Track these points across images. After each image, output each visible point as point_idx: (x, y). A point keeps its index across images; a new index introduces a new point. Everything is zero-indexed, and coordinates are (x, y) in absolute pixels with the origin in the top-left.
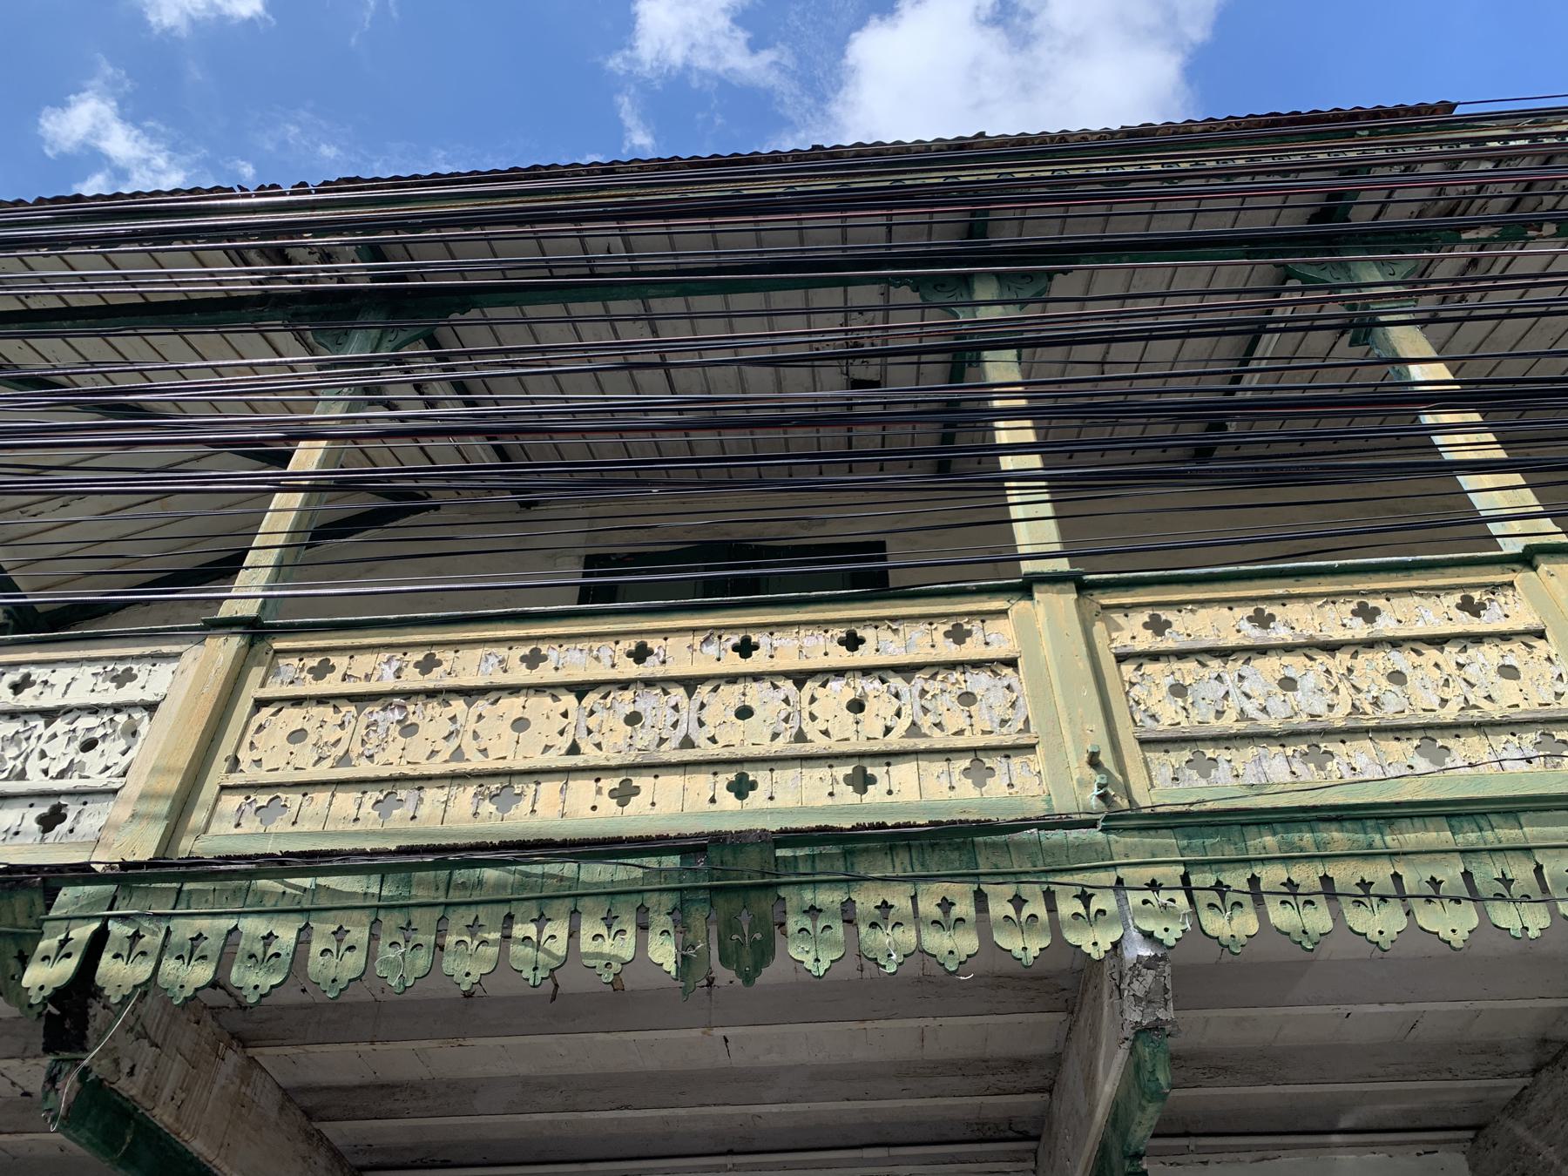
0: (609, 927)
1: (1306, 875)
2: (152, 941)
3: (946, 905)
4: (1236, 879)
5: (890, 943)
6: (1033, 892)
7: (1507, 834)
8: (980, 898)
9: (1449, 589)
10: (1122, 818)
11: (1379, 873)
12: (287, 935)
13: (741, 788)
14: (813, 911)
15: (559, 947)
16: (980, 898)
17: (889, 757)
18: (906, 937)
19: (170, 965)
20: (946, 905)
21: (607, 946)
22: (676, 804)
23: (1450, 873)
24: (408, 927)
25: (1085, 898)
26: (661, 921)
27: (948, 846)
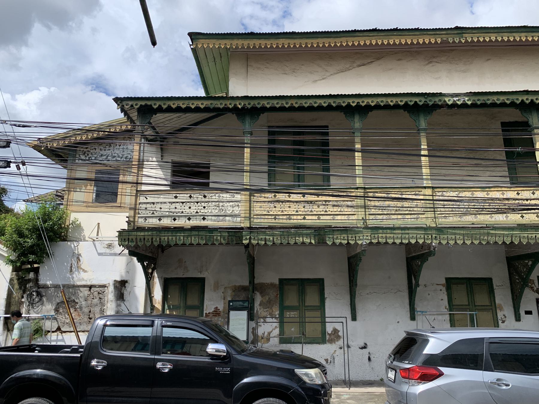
0: (46, 229)
1: (384, 235)
2: (256, 238)
3: (344, 237)
4: (376, 236)
5: (338, 242)
6: (354, 235)
7: (407, 232)
8: (348, 237)
9: (501, 191)
10: (367, 228)
11: (392, 235)
12: (271, 239)
13: (160, 220)
14: (329, 238)
15: (301, 240)
16: (348, 237)
17: (164, 217)
18: (339, 241)
19: (259, 242)
20: (344, 237)
21: (307, 241)
22: (311, 221)
23: (415, 236)
24: (284, 238)
25: (359, 237)
26: (313, 238)
27: (345, 230)
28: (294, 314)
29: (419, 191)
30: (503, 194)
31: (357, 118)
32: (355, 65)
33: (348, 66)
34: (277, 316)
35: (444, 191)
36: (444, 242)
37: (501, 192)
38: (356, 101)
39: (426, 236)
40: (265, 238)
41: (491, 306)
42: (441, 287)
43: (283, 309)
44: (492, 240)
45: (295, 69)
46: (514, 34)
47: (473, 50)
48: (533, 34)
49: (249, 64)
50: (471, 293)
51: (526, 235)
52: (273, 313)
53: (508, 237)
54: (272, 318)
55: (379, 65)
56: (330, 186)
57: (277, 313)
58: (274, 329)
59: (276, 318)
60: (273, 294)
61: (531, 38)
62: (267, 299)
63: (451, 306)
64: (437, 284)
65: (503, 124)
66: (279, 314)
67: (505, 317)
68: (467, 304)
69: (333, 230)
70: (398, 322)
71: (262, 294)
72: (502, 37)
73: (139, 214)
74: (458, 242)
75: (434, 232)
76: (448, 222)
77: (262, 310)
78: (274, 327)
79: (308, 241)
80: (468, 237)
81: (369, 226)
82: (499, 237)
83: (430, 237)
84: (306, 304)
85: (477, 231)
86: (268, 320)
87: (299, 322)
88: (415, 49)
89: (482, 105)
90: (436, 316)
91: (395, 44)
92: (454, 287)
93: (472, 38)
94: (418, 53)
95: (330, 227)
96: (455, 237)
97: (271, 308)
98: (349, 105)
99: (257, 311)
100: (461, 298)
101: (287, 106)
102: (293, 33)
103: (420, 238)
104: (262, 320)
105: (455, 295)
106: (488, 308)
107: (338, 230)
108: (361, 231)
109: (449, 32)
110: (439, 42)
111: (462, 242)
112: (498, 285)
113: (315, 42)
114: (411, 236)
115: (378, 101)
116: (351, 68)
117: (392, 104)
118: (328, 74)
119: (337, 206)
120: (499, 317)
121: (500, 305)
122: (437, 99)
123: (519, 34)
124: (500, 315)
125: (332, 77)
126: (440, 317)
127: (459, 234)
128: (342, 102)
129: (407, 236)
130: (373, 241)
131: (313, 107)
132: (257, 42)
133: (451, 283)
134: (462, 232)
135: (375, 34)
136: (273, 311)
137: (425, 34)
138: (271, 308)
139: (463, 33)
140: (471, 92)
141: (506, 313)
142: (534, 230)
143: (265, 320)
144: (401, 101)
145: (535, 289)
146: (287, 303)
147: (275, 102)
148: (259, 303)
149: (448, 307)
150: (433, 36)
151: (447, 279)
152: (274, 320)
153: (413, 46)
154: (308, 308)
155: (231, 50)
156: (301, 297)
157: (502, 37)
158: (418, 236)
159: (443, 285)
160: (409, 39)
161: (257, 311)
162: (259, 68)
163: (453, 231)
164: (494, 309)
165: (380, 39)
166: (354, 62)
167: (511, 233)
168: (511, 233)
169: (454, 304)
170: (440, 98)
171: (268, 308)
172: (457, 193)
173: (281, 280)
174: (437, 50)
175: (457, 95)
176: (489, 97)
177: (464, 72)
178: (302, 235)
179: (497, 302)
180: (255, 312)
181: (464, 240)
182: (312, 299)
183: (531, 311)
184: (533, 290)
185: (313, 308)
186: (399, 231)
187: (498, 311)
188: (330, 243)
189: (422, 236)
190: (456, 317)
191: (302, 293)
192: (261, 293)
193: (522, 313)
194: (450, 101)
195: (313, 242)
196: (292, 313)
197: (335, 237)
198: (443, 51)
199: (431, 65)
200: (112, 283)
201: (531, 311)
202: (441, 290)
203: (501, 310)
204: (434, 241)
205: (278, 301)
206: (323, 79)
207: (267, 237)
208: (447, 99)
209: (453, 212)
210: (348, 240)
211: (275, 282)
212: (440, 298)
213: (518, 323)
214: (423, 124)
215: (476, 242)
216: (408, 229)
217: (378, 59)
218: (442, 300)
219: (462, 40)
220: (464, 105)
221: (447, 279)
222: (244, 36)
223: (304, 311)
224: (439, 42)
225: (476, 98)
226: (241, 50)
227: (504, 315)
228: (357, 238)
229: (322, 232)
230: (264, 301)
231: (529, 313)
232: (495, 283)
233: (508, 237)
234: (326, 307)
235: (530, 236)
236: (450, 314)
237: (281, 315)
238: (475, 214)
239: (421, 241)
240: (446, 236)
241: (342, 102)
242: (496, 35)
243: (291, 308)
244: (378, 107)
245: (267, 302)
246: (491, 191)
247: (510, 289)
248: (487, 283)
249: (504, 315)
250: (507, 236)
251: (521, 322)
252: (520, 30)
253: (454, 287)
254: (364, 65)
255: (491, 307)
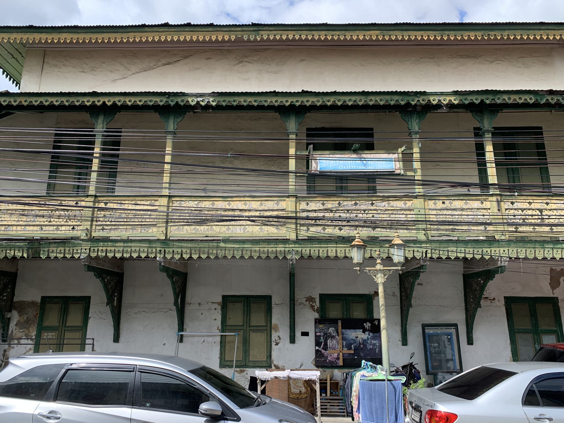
5: (52, 255)
6: (71, 248)
7: (130, 244)
14: (44, 251)
15: (13, 254)
18: (55, 255)
20: (60, 251)
21: (18, 254)
23: (138, 249)
25: (77, 250)
26: (25, 251)
27: (64, 241)
28: (52, 336)
29: (156, 200)
30: (277, 204)
31: (101, 119)
32: (160, 64)
33: (152, 65)
34: (34, 337)
35: (183, 201)
36: (169, 256)
37: (243, 202)
38: (92, 99)
39: (150, 250)
40: (106, 250)
41: (267, 326)
42: (216, 306)
43: (41, 329)
44: (221, 254)
45: (94, 67)
46: (314, 32)
47: (288, 49)
48: (333, 33)
49: (46, 61)
50: (247, 313)
51: (257, 249)
52: (29, 334)
53: (238, 250)
54: (28, 339)
55: (186, 64)
56: (376, 193)
57: (34, 334)
58: (28, 352)
59: (31, 339)
60: (32, 313)
61: (559, 37)
62: (25, 318)
63: (224, 327)
64: (213, 303)
65: (308, 129)
66: (36, 336)
67: (280, 339)
68: (242, 324)
69: (50, 243)
70: (164, 344)
71: (20, 313)
72: (300, 35)
73: (97, 221)
74: (184, 256)
75: (158, 245)
76: (180, 234)
77: (17, 331)
78: (28, 350)
79: (21, 254)
80: (195, 251)
81: (171, 238)
82: (229, 250)
83: (154, 250)
84: (251, 324)
85: (206, 245)
86: (22, 341)
87: (57, 344)
88: (226, 48)
89: (480, 106)
90: (206, 338)
91: (185, 40)
92: (230, 306)
93: (268, 35)
94: (229, 51)
95: (47, 239)
96: (182, 251)
97: (28, 329)
98: (408, 104)
99: (12, 331)
100: (236, 318)
101: (15, 104)
102: (76, 27)
103: (144, 252)
104: (16, 342)
105: (230, 315)
106: (239, 328)
107: (55, 242)
108: (81, 244)
109: (244, 29)
110: (233, 39)
111: (188, 256)
112: (277, 303)
113: (100, 37)
114: (133, 249)
115: (116, 100)
116: (155, 67)
117: (129, 104)
118: (130, 73)
119: (23, 215)
120: (273, 339)
121: (276, 325)
122: (179, 100)
123: (318, 32)
124: (274, 336)
125: (133, 75)
126: (210, 339)
127: (186, 247)
128: (75, 100)
129: (129, 249)
130: (67, 256)
131: (326, 105)
132: (37, 36)
133: (227, 301)
134: (189, 245)
135: (165, 29)
136: (29, 332)
137: (219, 31)
138: (28, 329)
139: (260, 30)
140: (213, 92)
141: (281, 334)
142: (273, 243)
143: (19, 342)
144: (140, 101)
145: (316, 308)
146: (46, 323)
147: (137, 99)
148: (15, 323)
149: (220, 328)
150: (227, 33)
151: (224, 297)
152: (30, 342)
153: (224, 45)
154: (69, 329)
155: (28, 45)
156: (62, 316)
157: (300, 35)
158: (142, 249)
159: (218, 304)
160: (201, 35)
161: (12, 331)
162: (56, 66)
163: (180, 244)
164: (269, 330)
165: (170, 35)
166: (159, 61)
167: (242, 246)
168: (242, 246)
169: (227, 324)
170: (183, 98)
171: (25, 328)
172: (196, 203)
173: (43, 298)
174: (250, 49)
175: (201, 95)
176: (236, 98)
177: (275, 73)
178: (14, 248)
179: (274, 321)
180: (10, 332)
181: (191, 254)
182: (74, 319)
183: (308, 333)
184: (314, 310)
185: (74, 329)
186: (122, 244)
187: (273, 332)
188: (43, 256)
189: (146, 250)
190: (228, 339)
191: (64, 312)
192: (19, 312)
193: (298, 334)
194: (192, 101)
195: (25, 255)
196: (50, 334)
197: (51, 249)
198: (256, 50)
199: (241, 64)
200: (557, 293)
201: (308, 333)
202: (215, 309)
203: (276, 331)
204: (158, 255)
205: (37, 321)
206: (124, 78)
207: (109, 249)
208: (431, 98)
209: (126, 223)
210: (64, 254)
211: (36, 300)
212: (214, 318)
213: (292, 345)
214: (171, 126)
215: (204, 256)
216: (132, 241)
217: (186, 57)
218: (215, 319)
219: (257, 37)
220: (208, 107)
221: (224, 297)
222: (24, 30)
223: (63, 331)
224: (233, 39)
225: (221, 99)
226: (39, 46)
227: (279, 337)
228: (75, 251)
229: (36, 245)
230: (21, 321)
231: (305, 334)
232: (274, 300)
233: (238, 250)
234: (88, 327)
235: (262, 249)
236: (221, 336)
237: (39, 336)
238: (277, 226)
239: (118, 255)
240: (171, 250)
241: (75, 100)
242: (294, 33)
243: (50, 329)
244: (20, 108)
245: (24, 322)
246: (233, 201)
247: (399, 307)
248: (266, 301)
249: (279, 337)
250: (238, 249)
251: (296, 345)
252: (320, 28)
253: (230, 306)
254: (169, 64)
255: (265, 328)
